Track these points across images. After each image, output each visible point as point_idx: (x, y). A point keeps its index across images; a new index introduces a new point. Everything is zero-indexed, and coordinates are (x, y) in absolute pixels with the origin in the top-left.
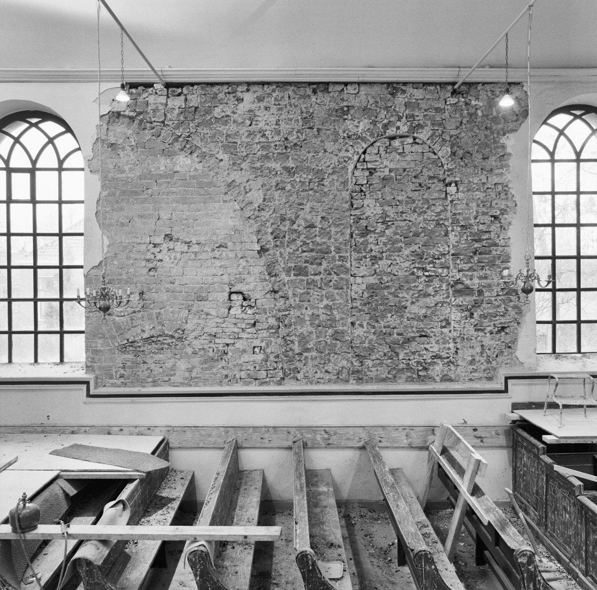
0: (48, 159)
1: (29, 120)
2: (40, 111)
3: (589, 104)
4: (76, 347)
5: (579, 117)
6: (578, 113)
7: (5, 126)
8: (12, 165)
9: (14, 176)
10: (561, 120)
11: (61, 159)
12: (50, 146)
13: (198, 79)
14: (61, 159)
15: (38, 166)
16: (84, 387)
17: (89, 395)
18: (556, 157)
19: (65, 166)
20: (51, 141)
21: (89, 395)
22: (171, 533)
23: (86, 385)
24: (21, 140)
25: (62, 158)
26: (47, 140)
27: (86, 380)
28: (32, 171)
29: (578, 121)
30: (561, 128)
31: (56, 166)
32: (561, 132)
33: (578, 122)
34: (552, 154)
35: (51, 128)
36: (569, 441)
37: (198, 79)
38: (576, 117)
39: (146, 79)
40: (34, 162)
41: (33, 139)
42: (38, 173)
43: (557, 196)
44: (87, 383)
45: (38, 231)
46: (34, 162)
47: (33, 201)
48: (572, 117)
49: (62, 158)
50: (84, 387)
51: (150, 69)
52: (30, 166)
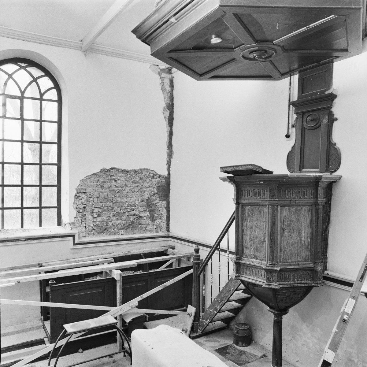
0: (33, 91)
5: (24, 68)
6: (23, 65)
10: (10, 68)
11: (23, 91)
14: (23, 91)
15: (25, 95)
16: (71, 238)
17: (75, 244)
19: (44, 97)
21: (75, 244)
22: (340, 53)
27: (72, 234)
28: (22, 98)
31: (39, 97)
36: (245, 168)
38: (21, 67)
40: (23, 93)
42: (25, 100)
43: (24, 139)
44: (73, 236)
45: (20, 139)
48: (18, 67)
49: (42, 92)
50: (71, 238)
52: (20, 95)
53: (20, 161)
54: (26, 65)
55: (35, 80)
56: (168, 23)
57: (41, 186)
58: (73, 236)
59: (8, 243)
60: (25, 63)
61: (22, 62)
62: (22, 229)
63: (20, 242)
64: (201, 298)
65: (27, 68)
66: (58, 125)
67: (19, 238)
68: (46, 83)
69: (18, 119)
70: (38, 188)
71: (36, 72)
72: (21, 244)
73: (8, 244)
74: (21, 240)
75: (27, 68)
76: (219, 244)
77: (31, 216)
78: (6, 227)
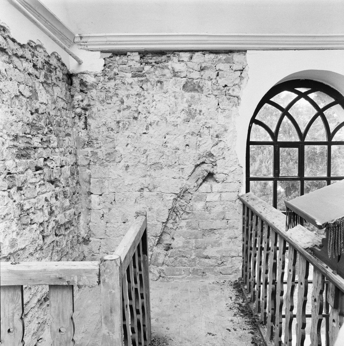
5: (304, 95)
6: (303, 90)
28: (300, 145)
32: (285, 112)
34: (274, 136)
38: (301, 95)
40: (302, 136)
46: (302, 136)
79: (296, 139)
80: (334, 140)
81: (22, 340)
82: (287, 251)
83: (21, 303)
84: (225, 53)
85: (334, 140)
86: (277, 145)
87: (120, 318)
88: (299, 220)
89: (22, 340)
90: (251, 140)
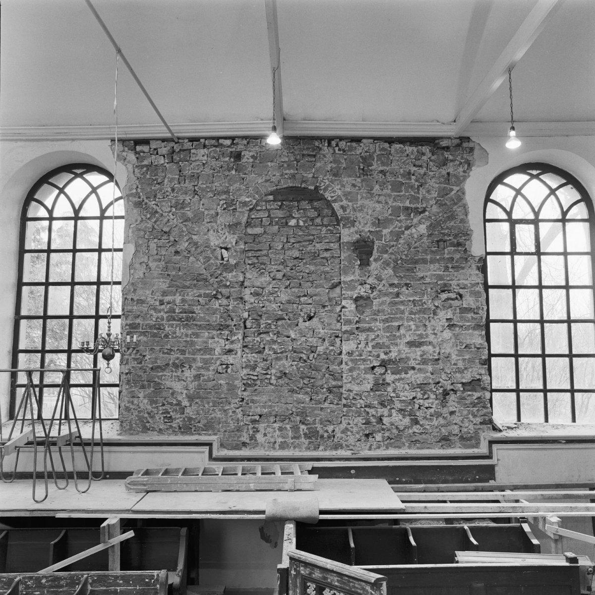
1: (530, 172)
2: (69, 165)
3: (60, 165)
4: (110, 402)
5: (537, 177)
6: (535, 172)
7: (49, 178)
8: (515, 216)
9: (518, 227)
12: (93, 195)
13: (390, 133)
15: (540, 217)
16: (206, 449)
18: (55, 215)
20: (94, 190)
21: (211, 457)
23: (208, 447)
24: (523, 191)
25: (104, 207)
26: (90, 190)
28: (536, 222)
29: (535, 181)
30: (517, 187)
31: (98, 214)
32: (518, 192)
33: (535, 182)
34: (509, 214)
35: (96, 178)
37: (390, 133)
38: (533, 177)
39: (346, 132)
40: (537, 214)
41: (77, 188)
44: (210, 445)
46: (537, 214)
47: (538, 253)
51: (163, 124)
53: (538, 318)
54: (538, 172)
55: (553, 192)
56: (5, 138)
57: (517, 356)
58: (210, 445)
59: (542, 444)
60: (537, 170)
61: (532, 169)
62: (573, 424)
63: (558, 444)
64: (114, 561)
65: (540, 177)
66: (592, 258)
67: (556, 439)
68: (568, 195)
69: (532, 254)
70: (513, 359)
71: (553, 181)
72: (507, 449)
73: (540, 447)
74: (560, 442)
75: (540, 177)
76: (35, 470)
77: (532, 403)
78: (523, 420)
79: (531, 216)
80: (568, 217)
81: (512, 111)
82: (387, 524)
83: (547, 383)
84: (88, 511)
85: (568, 217)
86: (513, 223)
87: (11, 333)
88: (112, 573)
89: (512, 111)
90: (487, 217)
